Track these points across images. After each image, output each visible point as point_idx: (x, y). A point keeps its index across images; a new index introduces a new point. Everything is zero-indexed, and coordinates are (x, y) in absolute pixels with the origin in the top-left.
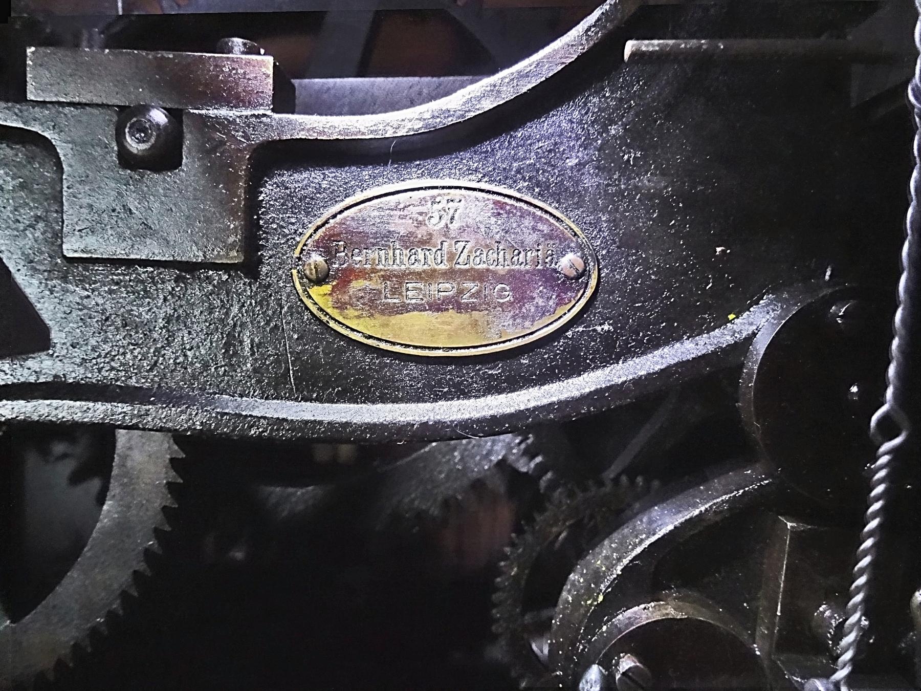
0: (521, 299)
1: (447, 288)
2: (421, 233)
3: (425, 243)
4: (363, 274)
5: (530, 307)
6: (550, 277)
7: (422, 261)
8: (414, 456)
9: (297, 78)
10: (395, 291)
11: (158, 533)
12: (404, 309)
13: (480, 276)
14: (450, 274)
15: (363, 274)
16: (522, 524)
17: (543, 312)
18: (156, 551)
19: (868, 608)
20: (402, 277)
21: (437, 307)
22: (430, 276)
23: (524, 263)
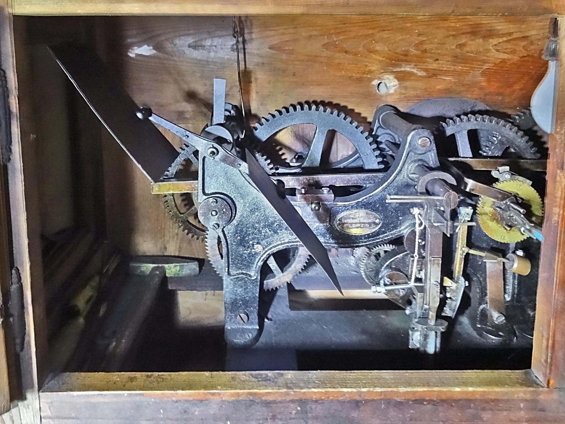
0: (370, 226)
1: (359, 225)
2: (355, 217)
3: (356, 218)
4: (346, 223)
5: (371, 227)
6: (374, 223)
7: (355, 221)
8: (364, 276)
9: (167, 263)
10: (351, 226)
11: (545, 143)
12: (353, 228)
13: (364, 223)
14: (360, 223)
15: (346, 223)
16: (300, 407)
17: (374, 228)
18: (553, 219)
19: (368, 391)
20: (352, 223)
21: (357, 228)
22: (356, 223)
23: (370, 221)
